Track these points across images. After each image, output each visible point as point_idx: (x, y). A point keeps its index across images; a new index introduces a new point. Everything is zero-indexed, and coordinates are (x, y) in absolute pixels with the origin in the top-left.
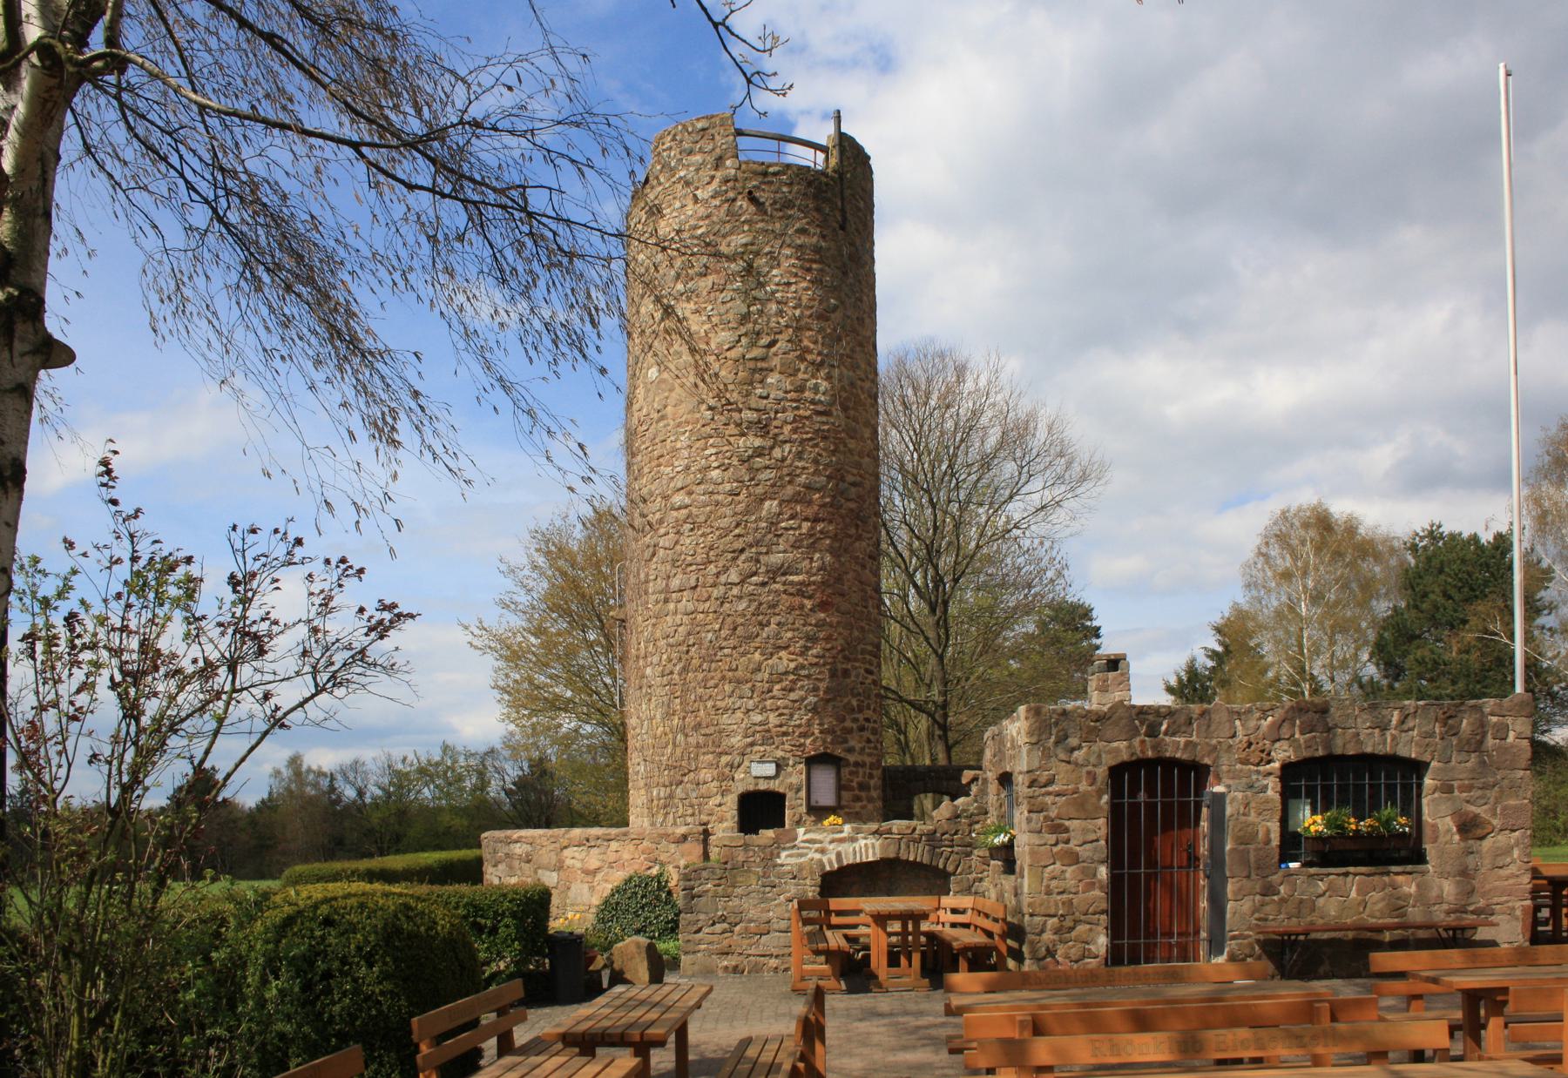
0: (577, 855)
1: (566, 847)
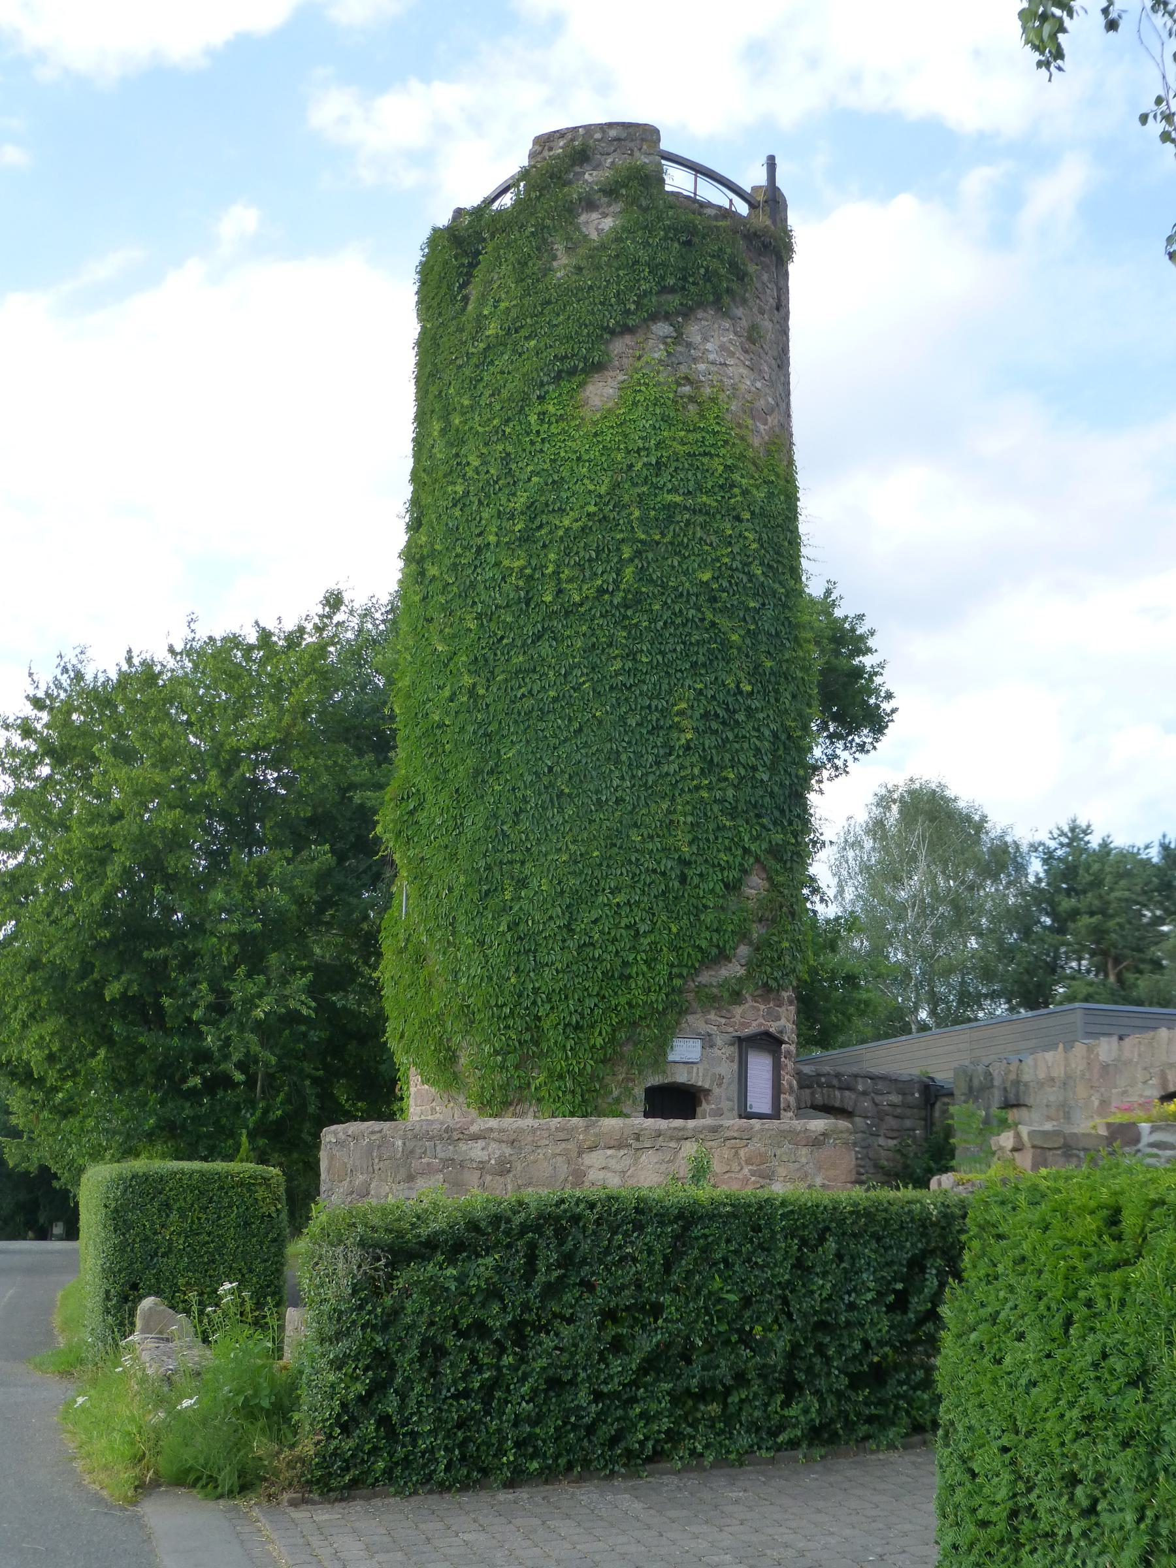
0: (612, 1163)
1: (591, 1149)
